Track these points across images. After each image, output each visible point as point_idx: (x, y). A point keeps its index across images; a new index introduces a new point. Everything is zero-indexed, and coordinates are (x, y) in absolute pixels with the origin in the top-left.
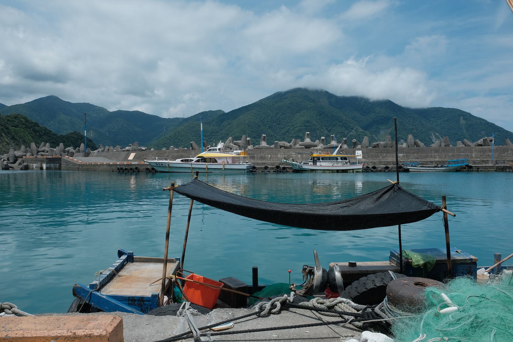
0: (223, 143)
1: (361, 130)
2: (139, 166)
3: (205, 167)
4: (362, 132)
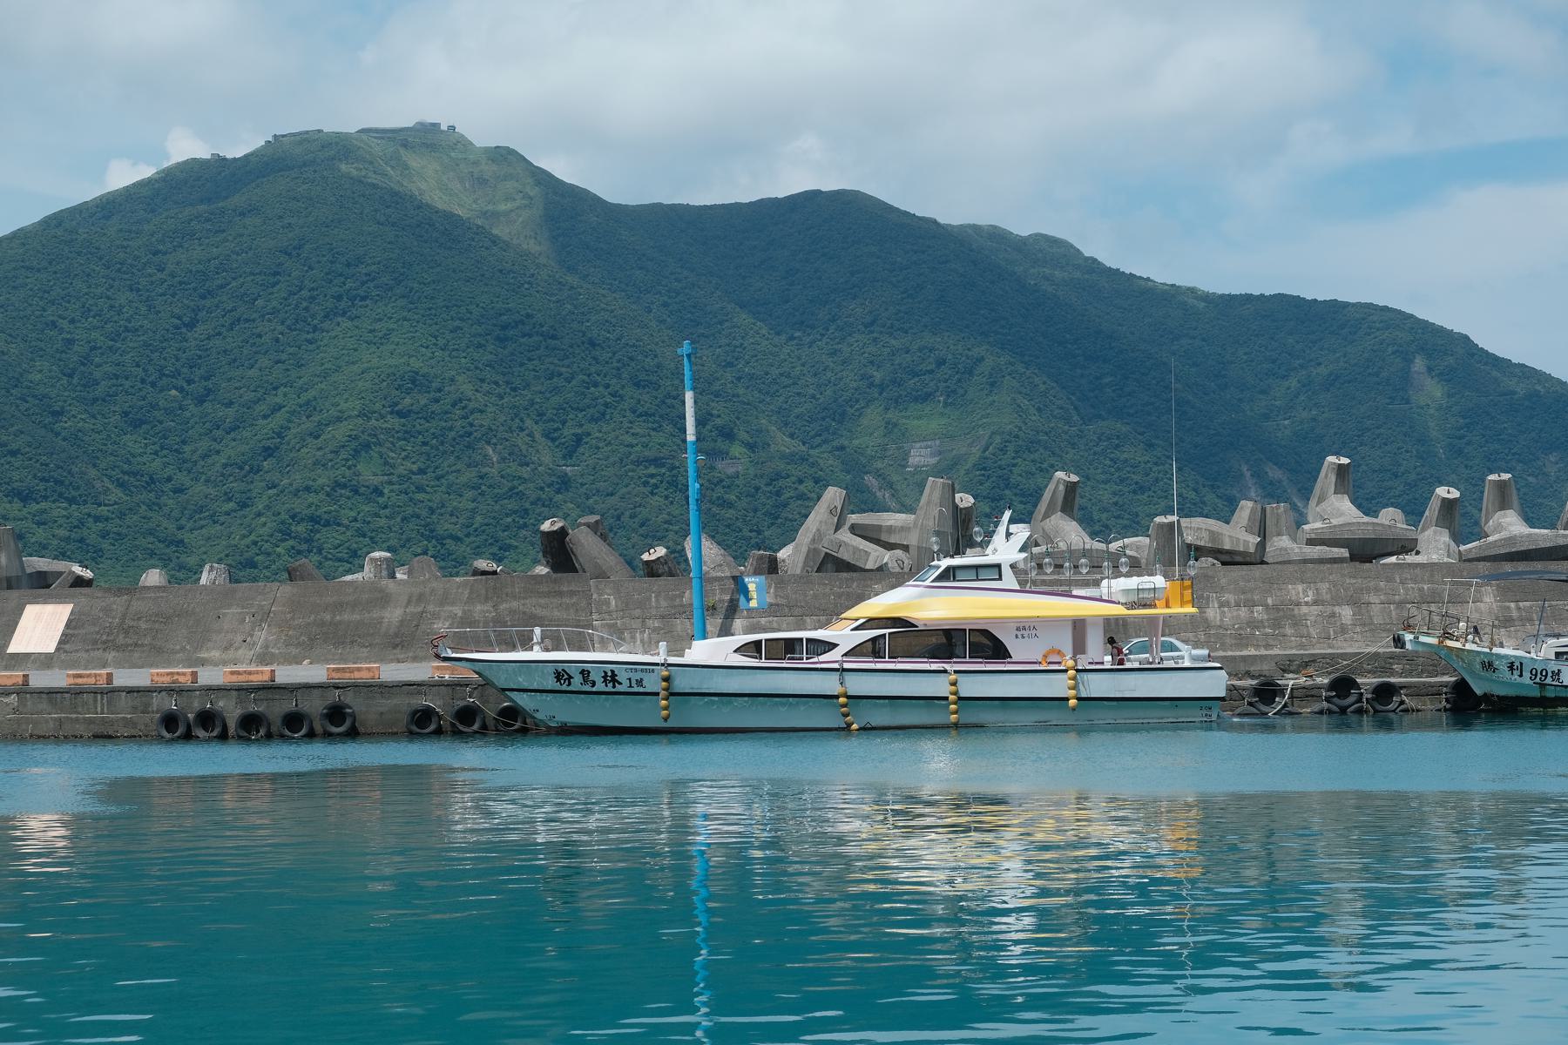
0: (1022, 532)
1: (783, 443)
2: (348, 698)
3: (938, 687)
4: (790, 458)
